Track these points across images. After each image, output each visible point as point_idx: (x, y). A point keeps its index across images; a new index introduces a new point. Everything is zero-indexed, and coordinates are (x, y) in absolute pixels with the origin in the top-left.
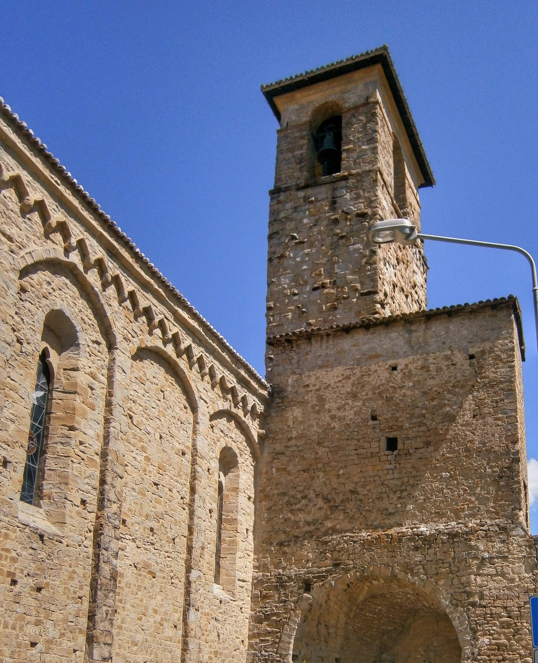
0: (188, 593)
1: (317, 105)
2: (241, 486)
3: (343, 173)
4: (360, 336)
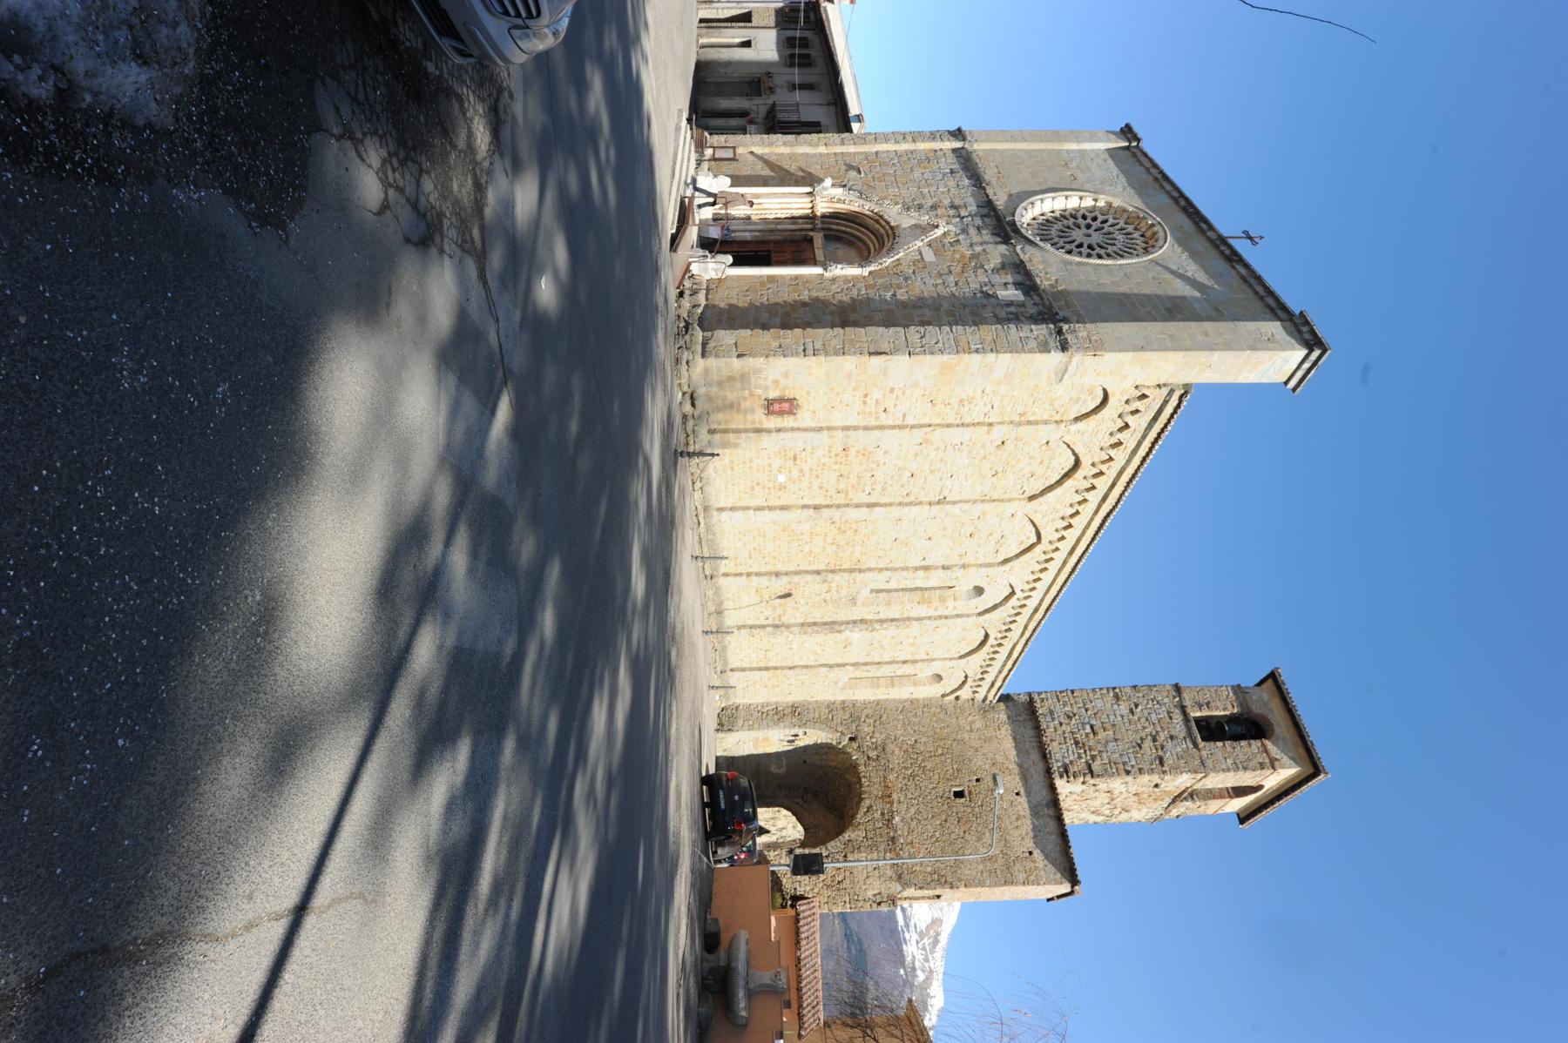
0: (838, 665)
3: (1202, 744)
4: (1041, 767)
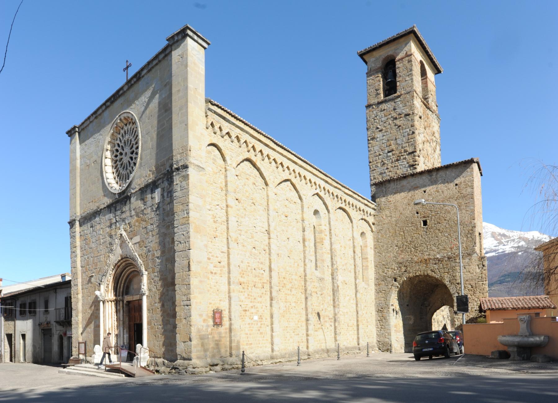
0: (356, 287)
1: (384, 57)
2: (368, 245)
4: (410, 179)
